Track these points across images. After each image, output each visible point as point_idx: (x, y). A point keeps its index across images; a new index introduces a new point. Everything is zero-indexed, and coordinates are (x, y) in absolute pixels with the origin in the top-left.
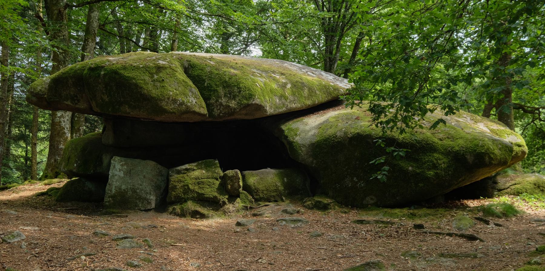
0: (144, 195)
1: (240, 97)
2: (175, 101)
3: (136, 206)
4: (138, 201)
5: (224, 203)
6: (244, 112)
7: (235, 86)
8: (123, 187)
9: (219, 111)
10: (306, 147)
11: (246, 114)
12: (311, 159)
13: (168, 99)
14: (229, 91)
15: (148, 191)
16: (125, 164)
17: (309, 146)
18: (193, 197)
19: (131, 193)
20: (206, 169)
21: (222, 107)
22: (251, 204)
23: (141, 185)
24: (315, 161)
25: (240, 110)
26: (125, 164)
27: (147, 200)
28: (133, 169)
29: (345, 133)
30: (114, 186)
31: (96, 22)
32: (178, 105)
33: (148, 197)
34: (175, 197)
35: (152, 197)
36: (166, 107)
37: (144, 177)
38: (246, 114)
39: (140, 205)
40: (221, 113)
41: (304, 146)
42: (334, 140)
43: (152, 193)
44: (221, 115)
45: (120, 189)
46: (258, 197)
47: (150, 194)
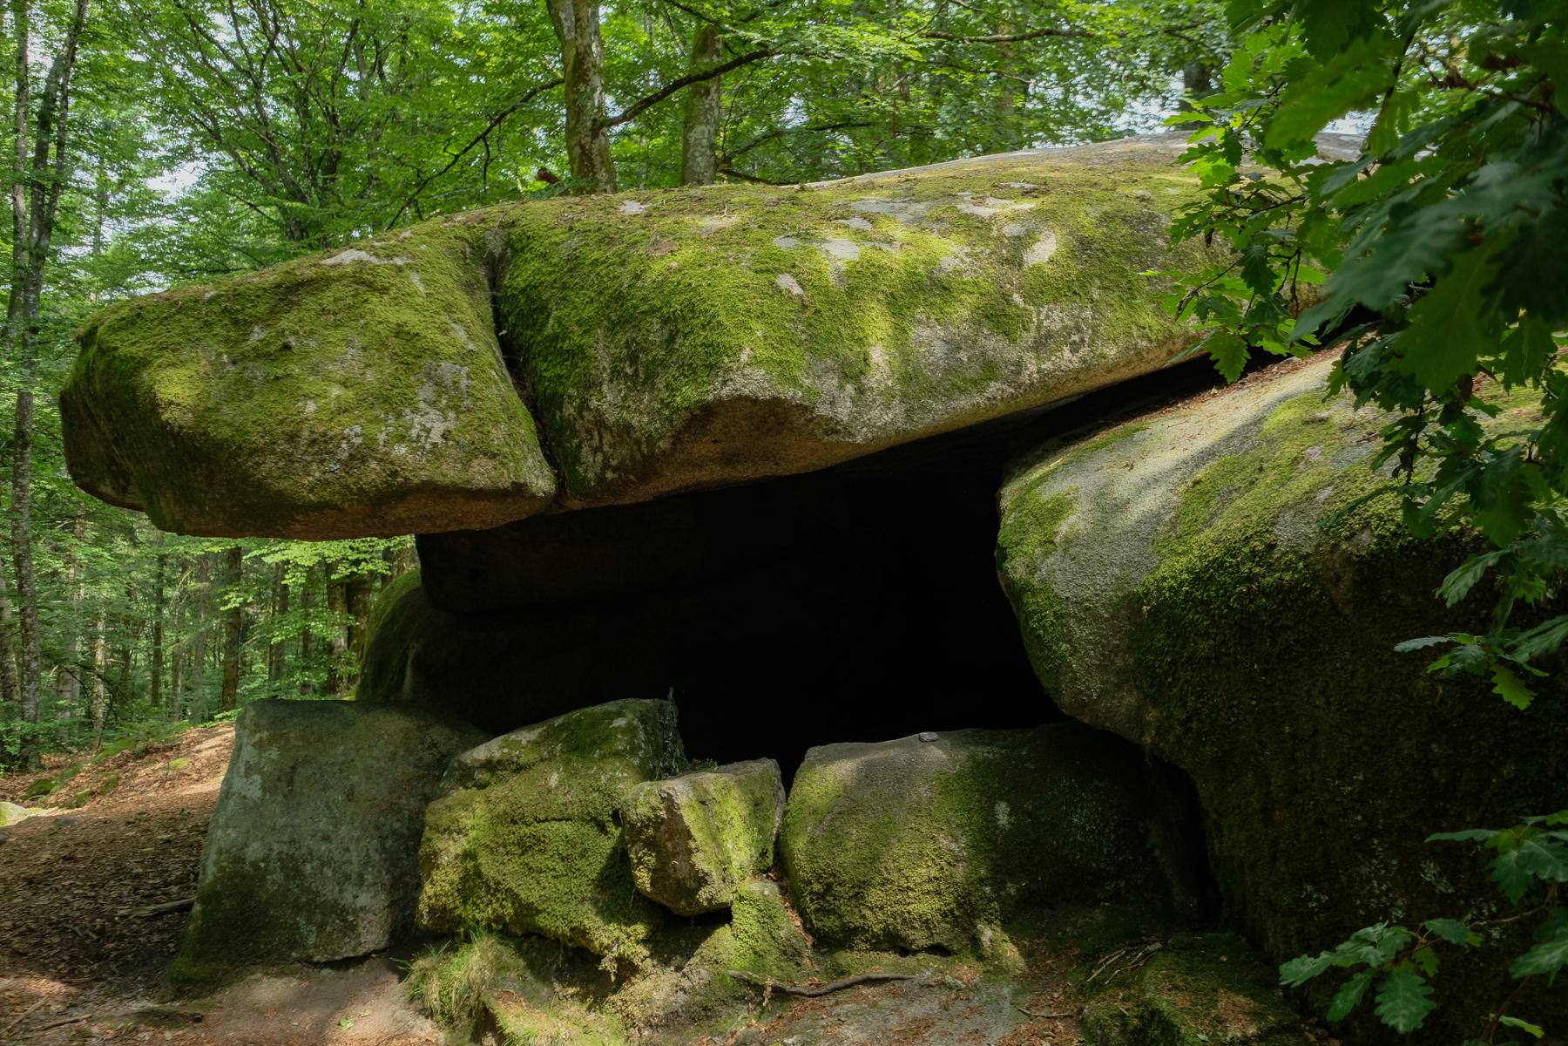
0: (329, 891)
1: (673, 371)
2: (322, 445)
3: (293, 945)
4: (301, 920)
5: (627, 969)
6: (703, 448)
7: (653, 311)
8: (254, 851)
9: (599, 457)
10: (1096, 618)
11: (729, 459)
12: (1130, 699)
13: (292, 438)
14: (628, 346)
15: (354, 868)
16: (272, 740)
17: (1116, 608)
18: (499, 919)
19: (278, 876)
20: (568, 762)
21: (607, 438)
22: (789, 967)
23: (326, 838)
24: (1151, 715)
25: (677, 440)
26: (272, 740)
27: (342, 912)
28: (306, 761)
29: (1332, 527)
30: (214, 848)
31: (702, 154)
32: (345, 464)
33: (348, 897)
34: (432, 910)
35: (364, 899)
36: (283, 485)
37: (350, 795)
38: (729, 459)
39: (312, 940)
40: (606, 466)
41: (1088, 613)
42: (1250, 579)
43: (369, 878)
44: (609, 475)
45: (240, 860)
46: (830, 923)
47: (361, 880)
